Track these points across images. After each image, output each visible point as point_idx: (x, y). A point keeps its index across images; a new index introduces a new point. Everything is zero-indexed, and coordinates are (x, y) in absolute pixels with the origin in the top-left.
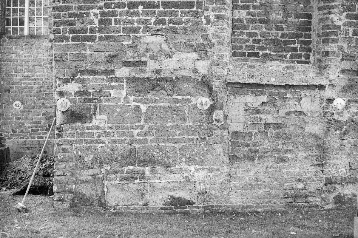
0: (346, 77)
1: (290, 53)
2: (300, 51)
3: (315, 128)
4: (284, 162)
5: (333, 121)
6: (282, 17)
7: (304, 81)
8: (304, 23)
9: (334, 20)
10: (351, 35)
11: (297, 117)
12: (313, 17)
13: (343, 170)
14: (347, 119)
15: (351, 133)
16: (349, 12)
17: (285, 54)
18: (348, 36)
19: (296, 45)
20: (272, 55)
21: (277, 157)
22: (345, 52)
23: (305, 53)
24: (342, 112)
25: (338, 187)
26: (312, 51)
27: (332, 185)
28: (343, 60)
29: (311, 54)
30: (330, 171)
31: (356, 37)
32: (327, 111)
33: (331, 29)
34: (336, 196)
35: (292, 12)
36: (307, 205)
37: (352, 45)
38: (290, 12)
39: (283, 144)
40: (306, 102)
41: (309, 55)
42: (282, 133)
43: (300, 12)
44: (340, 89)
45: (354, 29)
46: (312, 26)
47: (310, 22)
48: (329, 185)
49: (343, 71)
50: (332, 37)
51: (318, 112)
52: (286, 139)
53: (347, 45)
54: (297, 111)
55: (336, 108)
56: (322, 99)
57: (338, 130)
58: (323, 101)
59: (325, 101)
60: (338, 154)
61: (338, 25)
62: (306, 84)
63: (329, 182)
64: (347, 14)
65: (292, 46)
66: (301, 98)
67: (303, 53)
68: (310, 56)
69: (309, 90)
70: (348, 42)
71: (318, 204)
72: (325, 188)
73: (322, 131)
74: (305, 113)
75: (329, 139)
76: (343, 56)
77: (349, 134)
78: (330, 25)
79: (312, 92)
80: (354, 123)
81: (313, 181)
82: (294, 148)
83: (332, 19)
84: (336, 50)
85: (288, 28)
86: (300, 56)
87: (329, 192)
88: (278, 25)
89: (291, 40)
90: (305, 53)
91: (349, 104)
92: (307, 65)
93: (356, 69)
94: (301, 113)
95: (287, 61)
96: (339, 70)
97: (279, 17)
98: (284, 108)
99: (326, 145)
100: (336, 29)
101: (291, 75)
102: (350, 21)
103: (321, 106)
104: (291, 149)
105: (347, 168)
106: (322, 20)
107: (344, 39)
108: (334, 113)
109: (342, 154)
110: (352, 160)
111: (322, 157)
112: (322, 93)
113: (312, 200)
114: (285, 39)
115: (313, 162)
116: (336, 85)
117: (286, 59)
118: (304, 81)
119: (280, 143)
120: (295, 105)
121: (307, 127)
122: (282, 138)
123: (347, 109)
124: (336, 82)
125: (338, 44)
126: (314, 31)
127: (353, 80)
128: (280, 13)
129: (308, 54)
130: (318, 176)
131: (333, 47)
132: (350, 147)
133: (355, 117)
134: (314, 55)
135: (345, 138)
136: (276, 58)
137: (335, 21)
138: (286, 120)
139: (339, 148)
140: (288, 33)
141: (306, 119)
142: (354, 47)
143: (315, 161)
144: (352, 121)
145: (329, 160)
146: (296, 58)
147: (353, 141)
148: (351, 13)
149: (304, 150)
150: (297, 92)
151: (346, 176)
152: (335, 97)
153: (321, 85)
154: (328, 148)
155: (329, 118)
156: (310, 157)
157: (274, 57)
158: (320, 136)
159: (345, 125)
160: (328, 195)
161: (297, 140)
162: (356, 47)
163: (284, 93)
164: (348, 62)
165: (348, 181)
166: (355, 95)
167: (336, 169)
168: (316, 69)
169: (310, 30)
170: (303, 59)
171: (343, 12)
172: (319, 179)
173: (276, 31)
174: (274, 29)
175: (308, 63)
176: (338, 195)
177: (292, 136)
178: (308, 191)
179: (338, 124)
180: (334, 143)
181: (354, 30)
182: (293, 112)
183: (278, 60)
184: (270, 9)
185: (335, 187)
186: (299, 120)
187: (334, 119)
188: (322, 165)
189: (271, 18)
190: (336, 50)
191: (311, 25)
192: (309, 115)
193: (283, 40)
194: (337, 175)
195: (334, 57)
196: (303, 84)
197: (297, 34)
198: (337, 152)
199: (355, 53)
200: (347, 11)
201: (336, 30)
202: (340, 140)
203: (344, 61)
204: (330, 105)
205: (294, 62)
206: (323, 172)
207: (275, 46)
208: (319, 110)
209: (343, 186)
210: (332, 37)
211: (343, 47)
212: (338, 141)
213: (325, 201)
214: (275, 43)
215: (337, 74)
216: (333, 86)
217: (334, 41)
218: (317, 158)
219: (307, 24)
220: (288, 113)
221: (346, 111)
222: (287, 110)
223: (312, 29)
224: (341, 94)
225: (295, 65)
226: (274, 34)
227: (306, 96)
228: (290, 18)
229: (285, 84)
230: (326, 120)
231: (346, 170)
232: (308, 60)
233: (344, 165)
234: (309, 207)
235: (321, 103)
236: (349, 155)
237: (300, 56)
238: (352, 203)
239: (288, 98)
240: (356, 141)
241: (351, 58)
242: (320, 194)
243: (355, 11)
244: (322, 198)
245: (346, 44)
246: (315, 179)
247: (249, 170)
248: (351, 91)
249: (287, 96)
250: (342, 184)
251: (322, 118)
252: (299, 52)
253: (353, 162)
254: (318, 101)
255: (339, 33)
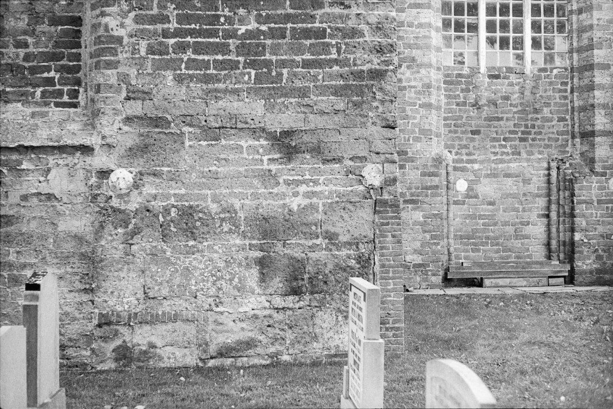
0: (134, 131)
1: (41, 89)
2: (60, 85)
3: (77, 223)
4: (20, 286)
5: (110, 210)
6: (28, 25)
7: (54, 138)
8: (65, 33)
9: (110, 27)
10: (143, 53)
11: (41, 203)
12: (83, 23)
13: (132, 299)
14: (138, 207)
15: (146, 231)
16: (141, 12)
17: (33, 90)
18: (137, 56)
19: (52, 74)
20: (8, 92)
21: (7, 276)
22: (131, 85)
23: (69, 88)
24: (128, 194)
25: (122, 331)
26: (83, 84)
27: (112, 327)
28: (129, 99)
29: (81, 90)
30: (106, 302)
31: (152, 57)
32: (99, 192)
33: (103, 43)
34: (118, 347)
35: (44, 15)
36: (65, 363)
37: (145, 72)
38: (41, 15)
39: (18, 252)
40: (58, 177)
41: (77, 92)
42: (16, 233)
43: (58, 14)
44: (122, 151)
45: (149, 42)
46: (82, 39)
47: (79, 31)
48: (106, 327)
49: (128, 120)
50: (107, 58)
51: (82, 195)
52: (23, 245)
53: (136, 72)
54: (41, 194)
55: (115, 187)
56: (88, 171)
57: (121, 226)
58: (89, 174)
59: (94, 174)
60: (121, 269)
61: (118, 36)
62: (56, 144)
63: (105, 322)
64: (136, 16)
65: (46, 75)
66: (49, 170)
67: (66, 89)
68: (79, 92)
69: (64, 155)
70: (139, 67)
71: (86, 361)
72: (98, 332)
73: (92, 229)
74: (57, 197)
75: (103, 243)
76: (128, 92)
77: (142, 234)
78: (103, 35)
79: (70, 159)
80: (151, 214)
81: (74, 319)
82: (37, 260)
83: (106, 26)
84: (113, 81)
85: (36, 44)
86: (60, 93)
87: (105, 339)
88: (19, 38)
89: (44, 65)
90: (69, 88)
91: (141, 180)
92: (72, 110)
93: (153, 116)
94: (50, 197)
95: (36, 103)
96: (119, 118)
97: (22, 24)
98: (18, 187)
99: (98, 254)
100: (113, 43)
101: (34, 129)
102: (141, 27)
103: (86, 184)
104: (32, 261)
105: (138, 296)
106: (95, 27)
107: (130, 60)
108: (111, 197)
109: (129, 270)
110: (148, 282)
111: (90, 275)
112: (88, 160)
113: (74, 355)
114: (31, 64)
115: (75, 285)
116: (115, 145)
117: (35, 100)
118: (54, 138)
119: (11, 250)
120: (40, 182)
121: (61, 222)
122: (15, 242)
123: (137, 189)
124: (113, 140)
125: (119, 70)
126: (86, 48)
127: (148, 135)
128: (23, 16)
129: (75, 90)
130: (83, 311)
131: (111, 76)
132: (144, 258)
133: (153, 203)
134: (86, 91)
135: (135, 240)
136: (14, 98)
137: (112, 30)
138: (23, 210)
139: (122, 260)
140: (36, 53)
141: (61, 207)
142: (149, 74)
143: (77, 282)
144: (148, 211)
145: (104, 281)
146: (53, 98)
147: (149, 247)
148: (144, 13)
149: (58, 263)
150: (41, 159)
151: (138, 310)
152: (112, 167)
153: (83, 145)
154: (102, 261)
155: (102, 206)
156: (68, 276)
157: (10, 96)
158: (88, 238)
159: (134, 218)
160: (103, 344)
161: (43, 245)
162: (154, 75)
163: (17, 160)
164: (139, 102)
165: (140, 320)
166: (152, 163)
167: (119, 298)
168: (88, 116)
169: (79, 46)
170: (66, 99)
171: (129, 11)
172: (85, 315)
173: (14, 50)
174: (11, 46)
175: (75, 106)
176: (120, 346)
177: (34, 238)
178: (66, 337)
179: (121, 216)
180: (114, 251)
181: (149, 44)
182: (34, 194)
183: (20, 101)
184: (5, 10)
185: (117, 331)
186: (46, 208)
187: (112, 207)
188: (92, 290)
189: (7, 27)
190: (113, 81)
191: (79, 38)
192: (65, 200)
193: (27, 65)
194: (119, 308)
195: (112, 95)
196: (51, 144)
197: (54, 54)
198: (120, 266)
199: (152, 86)
200: (137, 9)
201: (113, 46)
202: (124, 245)
203: (132, 102)
204: (105, 181)
205: (49, 104)
206: (93, 304)
207: (13, 76)
208: (83, 191)
209: (133, 329)
210: (107, 58)
211: (128, 75)
212: (121, 246)
213: (97, 356)
214: (12, 71)
215: (116, 126)
216: (110, 146)
217: (110, 65)
218: (83, 278)
219: (74, 35)
220: (25, 198)
221: (136, 192)
222: (24, 192)
223: (83, 45)
224: (126, 162)
225: (50, 109)
226: (11, 55)
227: (58, 165)
228: (42, 26)
229: (16, 144)
230: (98, 209)
231: (138, 299)
232: (75, 100)
233: (133, 290)
234: (70, 367)
235: (87, 179)
236: (143, 272)
237: (60, 93)
238: (147, 360)
239: (24, 169)
240: (156, 247)
241: (145, 95)
242: (89, 343)
243: (152, 9)
244: (93, 350)
245: (135, 70)
246: (78, 316)
247: (207, 393)
248: (145, 156)
249: (23, 167)
250: (129, 325)
251: (90, 205)
252: (58, 87)
253: (150, 285)
254: (81, 174)
255: (119, 50)
